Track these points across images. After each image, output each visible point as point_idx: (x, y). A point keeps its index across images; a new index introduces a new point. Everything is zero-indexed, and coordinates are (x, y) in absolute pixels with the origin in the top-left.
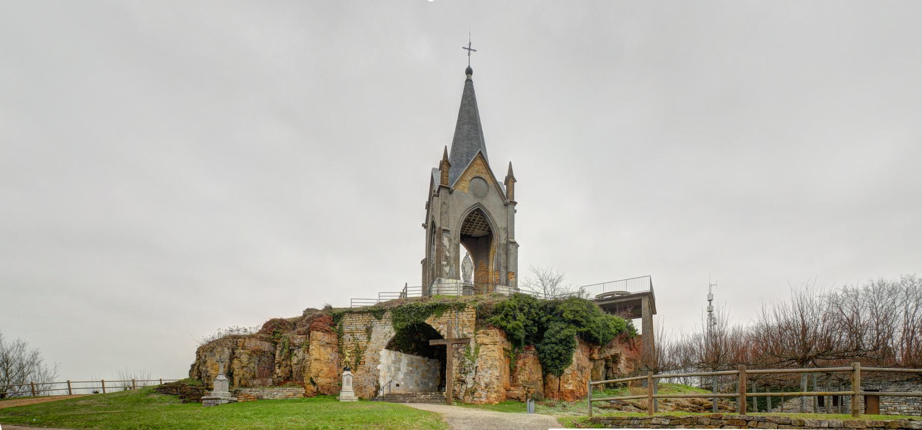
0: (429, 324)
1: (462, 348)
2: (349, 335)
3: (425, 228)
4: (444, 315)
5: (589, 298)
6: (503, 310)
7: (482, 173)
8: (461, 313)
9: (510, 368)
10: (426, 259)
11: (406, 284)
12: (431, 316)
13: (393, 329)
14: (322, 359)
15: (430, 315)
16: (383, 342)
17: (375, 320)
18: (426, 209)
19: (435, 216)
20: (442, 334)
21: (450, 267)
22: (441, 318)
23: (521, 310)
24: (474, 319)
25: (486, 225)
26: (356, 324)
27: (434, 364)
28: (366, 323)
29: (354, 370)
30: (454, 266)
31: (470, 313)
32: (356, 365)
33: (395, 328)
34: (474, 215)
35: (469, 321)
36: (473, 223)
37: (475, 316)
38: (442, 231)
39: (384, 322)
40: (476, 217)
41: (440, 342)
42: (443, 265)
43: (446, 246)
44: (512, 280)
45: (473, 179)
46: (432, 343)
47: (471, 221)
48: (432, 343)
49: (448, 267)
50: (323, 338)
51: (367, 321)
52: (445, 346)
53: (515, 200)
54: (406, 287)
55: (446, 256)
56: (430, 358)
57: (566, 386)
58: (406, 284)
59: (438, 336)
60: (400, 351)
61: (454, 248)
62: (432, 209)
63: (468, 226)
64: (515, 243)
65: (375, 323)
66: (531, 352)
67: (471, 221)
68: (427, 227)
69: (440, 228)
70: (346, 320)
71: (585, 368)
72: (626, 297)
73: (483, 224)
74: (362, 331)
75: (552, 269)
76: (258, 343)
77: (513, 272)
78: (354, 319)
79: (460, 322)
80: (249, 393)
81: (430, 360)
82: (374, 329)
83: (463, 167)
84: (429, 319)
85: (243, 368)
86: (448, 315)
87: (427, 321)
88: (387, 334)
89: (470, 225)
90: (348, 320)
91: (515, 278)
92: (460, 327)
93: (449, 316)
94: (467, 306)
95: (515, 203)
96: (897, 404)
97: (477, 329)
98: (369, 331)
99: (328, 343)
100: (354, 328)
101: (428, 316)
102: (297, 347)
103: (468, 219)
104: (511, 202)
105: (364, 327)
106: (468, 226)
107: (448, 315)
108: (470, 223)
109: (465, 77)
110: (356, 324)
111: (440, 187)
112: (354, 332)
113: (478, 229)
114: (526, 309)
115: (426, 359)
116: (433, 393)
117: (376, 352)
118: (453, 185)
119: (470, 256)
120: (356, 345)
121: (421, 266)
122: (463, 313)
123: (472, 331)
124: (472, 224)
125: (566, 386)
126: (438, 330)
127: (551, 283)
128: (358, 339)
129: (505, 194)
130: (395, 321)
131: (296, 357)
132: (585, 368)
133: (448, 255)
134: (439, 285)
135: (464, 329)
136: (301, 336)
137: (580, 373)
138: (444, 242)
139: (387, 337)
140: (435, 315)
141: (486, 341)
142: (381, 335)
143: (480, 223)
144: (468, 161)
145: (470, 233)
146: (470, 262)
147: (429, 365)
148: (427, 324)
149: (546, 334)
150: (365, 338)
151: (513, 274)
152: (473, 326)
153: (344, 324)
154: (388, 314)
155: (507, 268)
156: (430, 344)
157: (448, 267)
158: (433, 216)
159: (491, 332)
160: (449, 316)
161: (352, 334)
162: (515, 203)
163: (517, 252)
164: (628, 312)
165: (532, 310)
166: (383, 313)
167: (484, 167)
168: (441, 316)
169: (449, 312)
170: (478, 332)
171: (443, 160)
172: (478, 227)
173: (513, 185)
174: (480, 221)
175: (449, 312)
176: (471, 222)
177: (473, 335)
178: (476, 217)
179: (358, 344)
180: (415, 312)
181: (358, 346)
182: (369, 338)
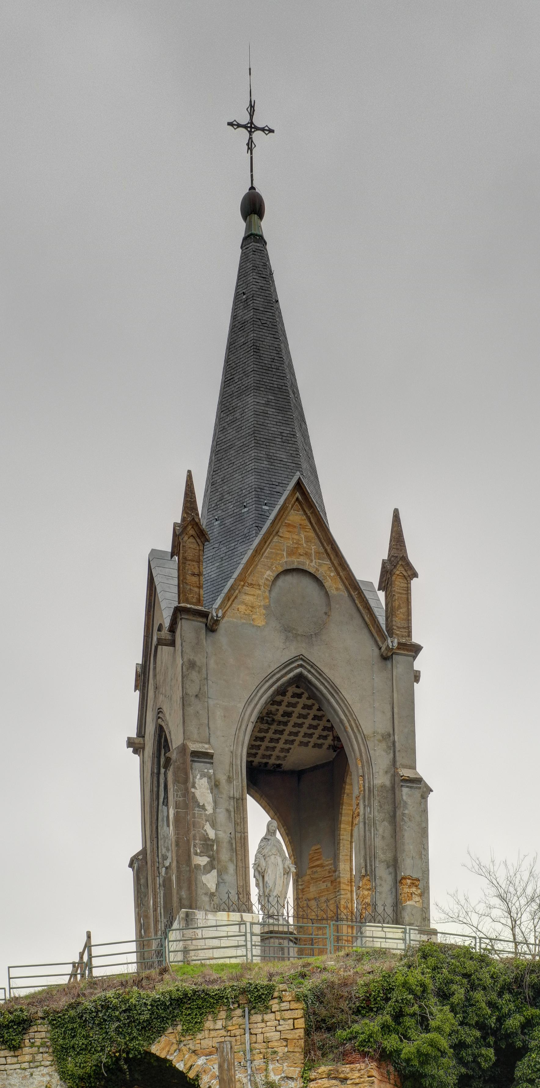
3: (135, 752)
4: (209, 1024)
6: (387, 999)
7: (307, 554)
8: (258, 1018)
10: (144, 852)
11: (89, 936)
13: (56, 1076)
15: (164, 1029)
18: (136, 688)
19: (165, 709)
21: (220, 874)
22: (199, 1036)
23: (444, 996)
30: (231, 868)
31: (287, 1015)
35: (286, 1040)
37: (301, 1023)
38: (189, 758)
42: (197, 867)
43: (203, 807)
44: (412, 904)
45: (278, 576)
49: (214, 873)
53: (416, 639)
54: (88, 946)
55: (206, 839)
58: (89, 936)
61: (228, 811)
62: (156, 688)
64: (419, 780)
68: (143, 748)
69: (183, 748)
77: (415, 876)
79: (256, 1045)
83: (247, 539)
84: (163, 1039)
91: (421, 895)
92: (259, 1062)
93: (224, 1027)
94: (276, 994)
95: (416, 649)
101: (161, 1032)
104: (402, 646)
107: (219, 1024)
109: (240, 227)
111: (178, 612)
114: (459, 994)
118: (219, 601)
121: (129, 874)
122: (267, 1017)
123: (295, 1071)
126: (191, 1075)
129: (382, 621)
133: (211, 834)
135: (271, 1067)
140: (179, 1028)
144: (262, 517)
148: (158, 1058)
151: (415, 882)
152: (299, 1057)
155: (394, 864)
157: (214, 873)
158: (160, 711)
159: (352, 1070)
162: (416, 649)
163: (424, 812)
165: (478, 995)
166: (25, 1030)
167: (312, 534)
168: (200, 1030)
169: (223, 1014)
170: (313, 1075)
171: (183, 519)
173: (408, 590)
175: (223, 1014)
180: (119, 1020)
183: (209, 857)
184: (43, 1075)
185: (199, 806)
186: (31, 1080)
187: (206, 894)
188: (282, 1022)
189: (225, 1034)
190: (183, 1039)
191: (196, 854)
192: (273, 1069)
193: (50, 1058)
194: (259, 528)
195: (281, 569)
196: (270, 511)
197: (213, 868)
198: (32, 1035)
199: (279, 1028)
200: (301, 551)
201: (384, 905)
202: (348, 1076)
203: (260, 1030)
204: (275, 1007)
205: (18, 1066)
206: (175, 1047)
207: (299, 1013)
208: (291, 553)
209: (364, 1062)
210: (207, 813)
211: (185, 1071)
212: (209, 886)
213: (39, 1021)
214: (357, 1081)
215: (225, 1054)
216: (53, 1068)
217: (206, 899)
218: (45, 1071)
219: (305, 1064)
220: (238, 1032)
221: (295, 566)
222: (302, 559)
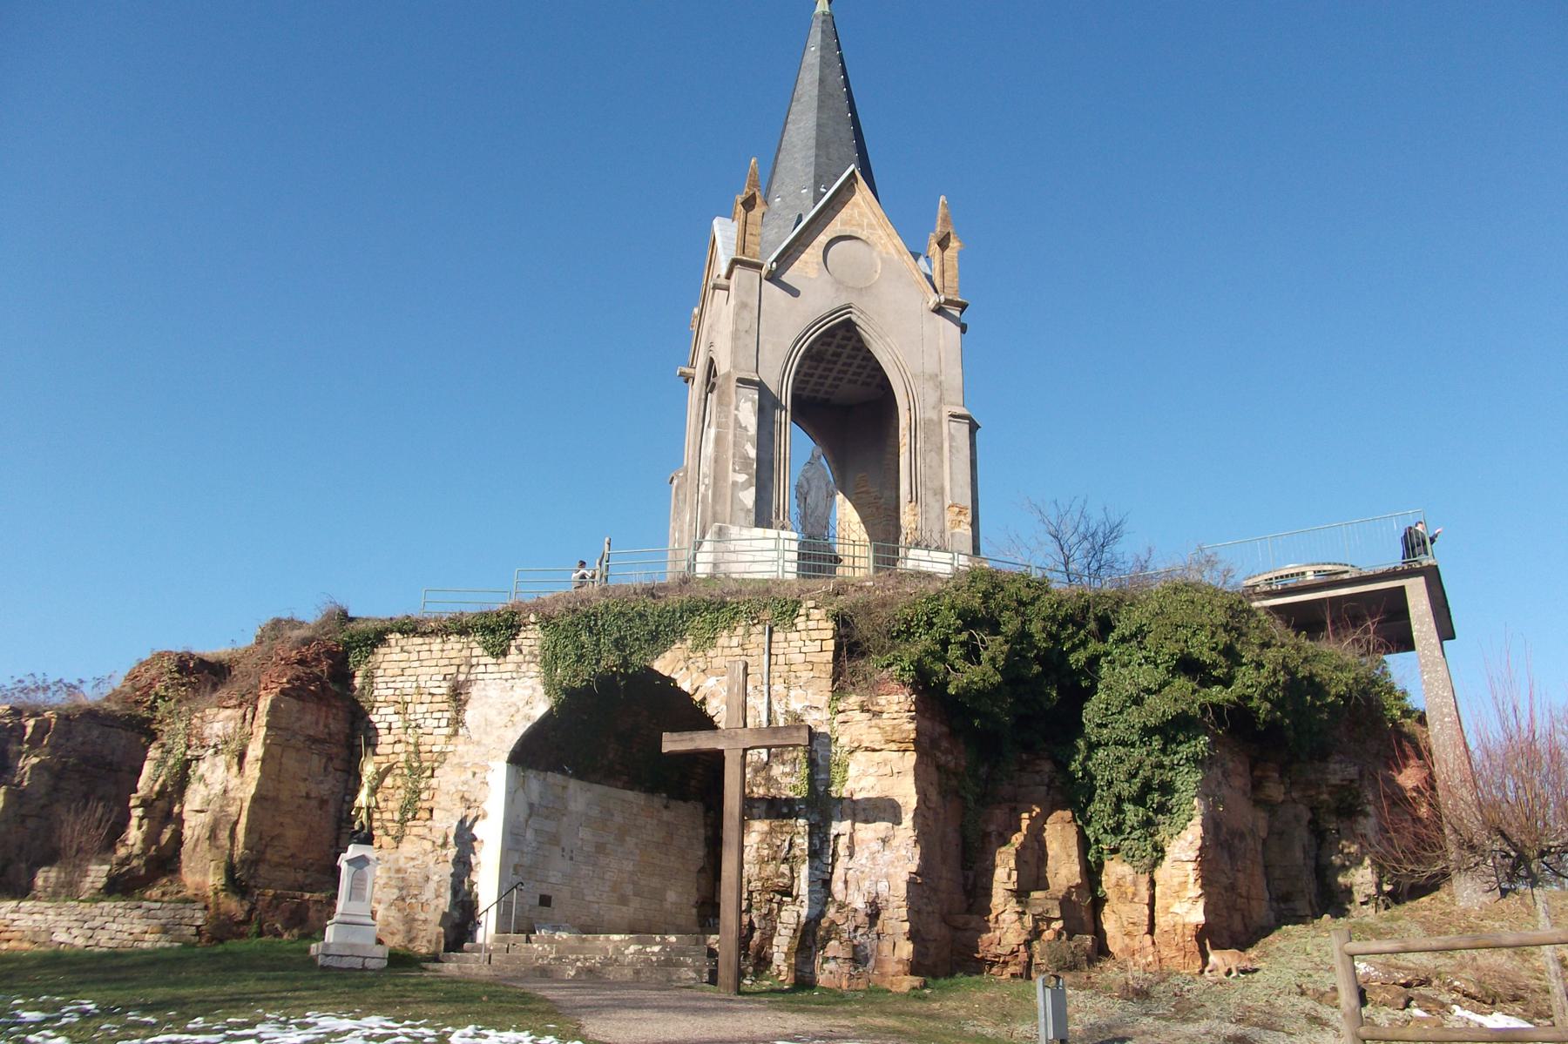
0: (666, 674)
1: (36, 756)
2: (391, 710)
5: (1232, 582)
7: (860, 226)
9: (964, 838)
12: (678, 645)
14: (284, 795)
16: (501, 739)
17: (483, 660)
20: (710, 711)
22: (711, 653)
24: (829, 656)
25: (873, 369)
26: (419, 671)
27: (686, 815)
28: (453, 669)
29: (395, 838)
31: (815, 635)
32: (403, 822)
33: (550, 687)
34: (837, 340)
36: (835, 363)
37: (830, 645)
39: (511, 667)
40: (843, 347)
41: (701, 741)
42: (735, 484)
43: (745, 429)
46: (672, 743)
47: (828, 356)
48: (672, 743)
49: (753, 490)
50: (299, 719)
51: (457, 661)
52: (717, 757)
56: (671, 796)
57: (1176, 908)
59: (694, 716)
60: (564, 772)
63: (819, 372)
65: (482, 668)
66: (1038, 778)
67: (828, 356)
69: (728, 376)
70: (387, 658)
71: (1242, 836)
72: (321, 1005)
73: (864, 367)
74: (435, 699)
75: (1085, 502)
76: (96, 733)
77: (963, 505)
78: (414, 656)
80: (10, 916)
81: (673, 803)
82: (474, 691)
84: (668, 654)
85: (23, 821)
86: (735, 642)
87: (662, 665)
88: (518, 711)
89: (825, 370)
90: (395, 657)
93: (741, 645)
96: (384, 685)
97: (838, 691)
98: (458, 694)
99: (314, 740)
100: (409, 687)
101: (665, 648)
102: (211, 751)
103: (819, 352)
105: (444, 684)
106: (819, 372)
107: (735, 642)
108: (823, 365)
110: (419, 671)
112: (408, 699)
113: (850, 381)
115: (658, 800)
116: (673, 939)
117: (474, 774)
118: (774, 256)
119: (823, 460)
120: (411, 748)
123: (823, 699)
124: (830, 366)
125: (1176, 908)
126: (698, 698)
127: (1086, 545)
128: (418, 726)
130: (550, 662)
131: (201, 787)
132: (1242, 836)
134: (721, 546)
136: (228, 712)
137: (1226, 856)
138: (741, 417)
139: (516, 719)
140: (689, 642)
141: (873, 737)
142: (500, 713)
143: (852, 370)
145: (826, 393)
146: (825, 475)
147: (668, 824)
149: (1091, 711)
150: (444, 722)
153: (380, 672)
154: (531, 638)
156: (665, 750)
160: (741, 645)
161: (402, 707)
164: (1366, 631)
169: (740, 631)
172: (849, 376)
174: (854, 357)
176: (829, 362)
177: (826, 714)
178: (843, 347)
179: (417, 745)
181: (418, 753)
182: (457, 723)
183: (748, 474)
184: (525, 688)
185: (741, 427)
186: (511, 693)
187: (741, 510)
188: (808, 643)
189: (741, 652)
190: (691, 655)
191: (734, 471)
192: (795, 696)
193: (537, 669)
194: (816, 204)
195: (834, 235)
196: (824, 194)
197: (751, 486)
198: (519, 642)
199: (803, 650)
200: (854, 222)
201: (931, 531)
202: (885, 709)
203: (782, 651)
204: (801, 626)
205: (499, 675)
206: (682, 664)
207: (830, 634)
208: (844, 223)
209: (903, 694)
210: (749, 434)
211: (691, 692)
212: (746, 502)
213: (530, 627)
214: (895, 715)
215: (736, 675)
216: (538, 680)
217: (742, 515)
218: (529, 682)
219: (832, 692)
220: (755, 652)
221: (848, 233)
222: (854, 228)
